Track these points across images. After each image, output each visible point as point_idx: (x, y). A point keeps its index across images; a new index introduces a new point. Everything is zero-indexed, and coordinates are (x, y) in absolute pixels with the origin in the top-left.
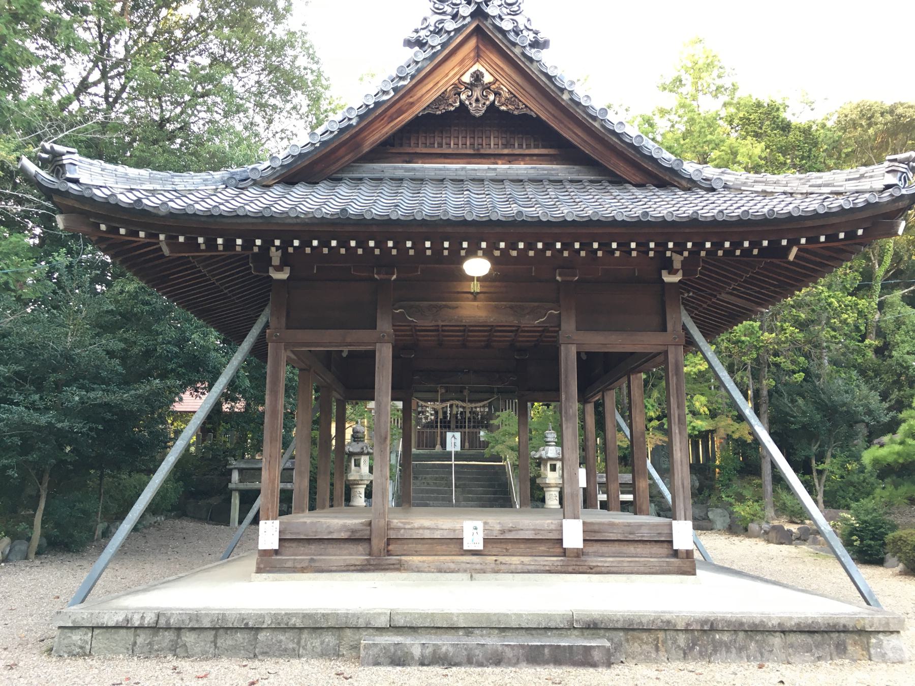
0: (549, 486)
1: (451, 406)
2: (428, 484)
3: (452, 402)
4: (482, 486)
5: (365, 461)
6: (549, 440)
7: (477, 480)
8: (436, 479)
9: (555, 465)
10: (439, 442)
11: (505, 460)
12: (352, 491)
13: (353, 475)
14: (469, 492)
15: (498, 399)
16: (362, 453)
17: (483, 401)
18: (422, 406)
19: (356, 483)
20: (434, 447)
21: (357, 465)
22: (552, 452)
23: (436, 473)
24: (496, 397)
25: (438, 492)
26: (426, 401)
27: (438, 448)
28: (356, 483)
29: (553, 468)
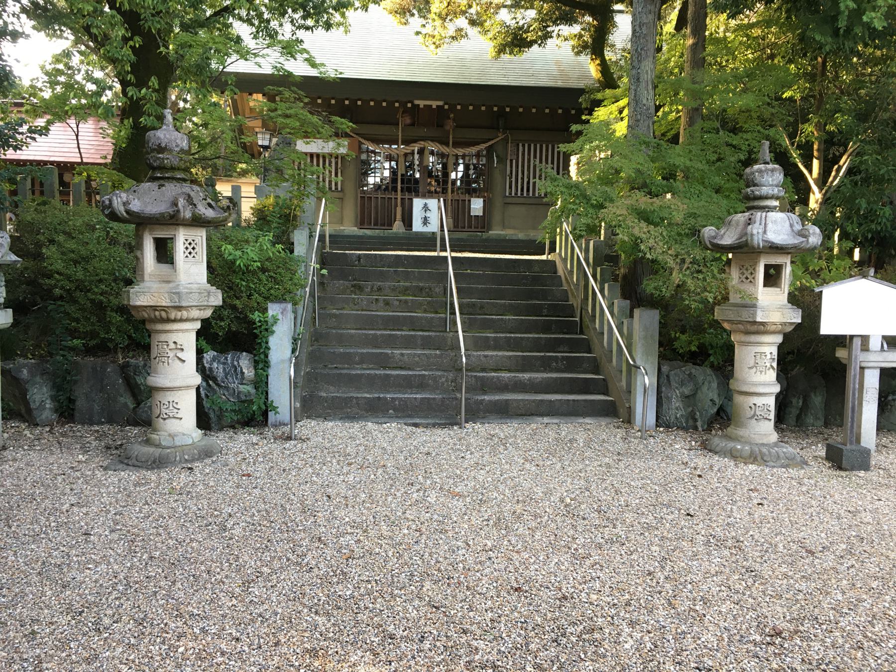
0: (759, 329)
1: (421, 152)
2: (387, 303)
3: (422, 144)
4: (516, 311)
5: (191, 248)
6: (765, 190)
7: (500, 295)
8: (405, 291)
9: (778, 268)
10: (399, 216)
11: (553, 249)
12: (156, 339)
13: (146, 294)
14: (487, 325)
15: (506, 140)
16: (173, 220)
17: (478, 144)
18: (368, 151)
19: (162, 316)
20: (390, 225)
21: (165, 253)
22: (777, 227)
23: (407, 276)
24: (501, 136)
25: (412, 324)
26: (377, 141)
27: (398, 227)
28: (162, 316)
29: (772, 278)
